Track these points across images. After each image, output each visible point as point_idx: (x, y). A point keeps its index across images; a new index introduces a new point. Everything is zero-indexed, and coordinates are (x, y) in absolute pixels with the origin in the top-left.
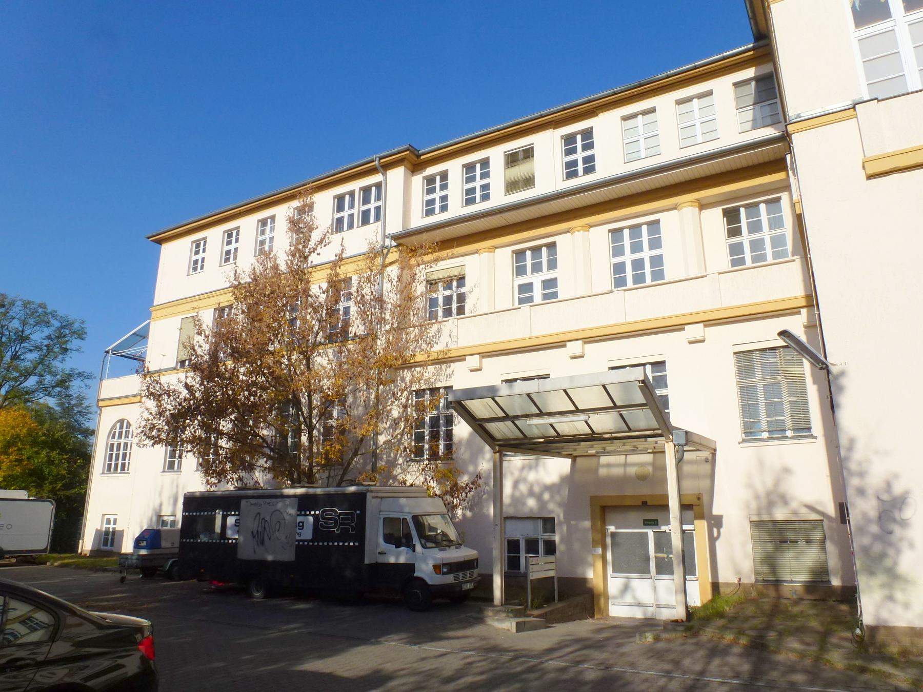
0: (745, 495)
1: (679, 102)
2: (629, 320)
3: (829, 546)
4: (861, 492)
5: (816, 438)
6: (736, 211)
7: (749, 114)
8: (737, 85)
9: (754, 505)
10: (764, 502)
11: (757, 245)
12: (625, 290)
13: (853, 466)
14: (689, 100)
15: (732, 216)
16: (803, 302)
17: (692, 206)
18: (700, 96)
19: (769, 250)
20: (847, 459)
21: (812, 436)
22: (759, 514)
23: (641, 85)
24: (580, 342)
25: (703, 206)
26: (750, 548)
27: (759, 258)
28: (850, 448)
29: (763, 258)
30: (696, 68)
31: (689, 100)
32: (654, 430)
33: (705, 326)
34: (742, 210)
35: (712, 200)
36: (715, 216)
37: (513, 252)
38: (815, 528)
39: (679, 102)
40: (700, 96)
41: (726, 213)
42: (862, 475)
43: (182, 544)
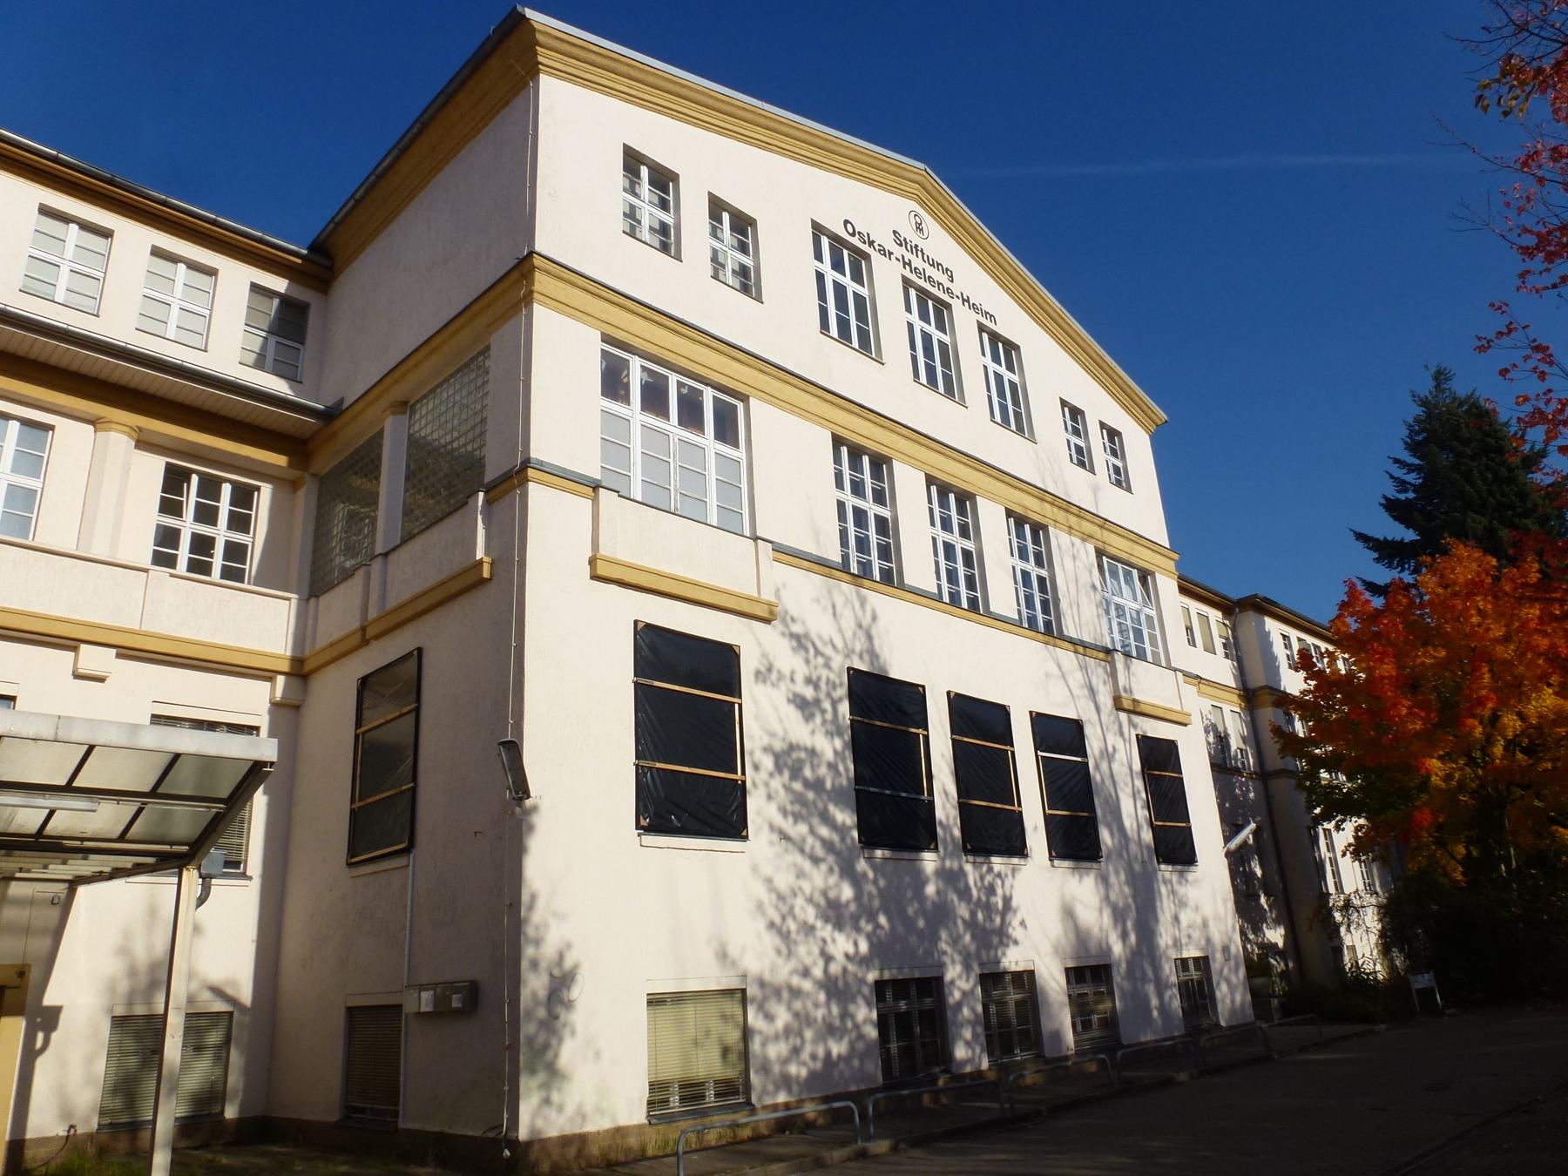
0: (112, 966)
1: (157, 252)
2: (146, 628)
3: (235, 1057)
4: (535, 965)
5: (250, 878)
6: (185, 475)
7: (256, 344)
8: (256, 288)
9: (123, 986)
10: (143, 980)
11: (202, 545)
12: (172, 575)
13: (530, 931)
14: (173, 259)
15: (174, 480)
16: (286, 668)
17: (129, 435)
18: (193, 266)
19: (218, 561)
20: (527, 921)
21: (244, 876)
22: (130, 1004)
23: (111, 182)
24: (114, 651)
25: (145, 443)
26: (100, 1066)
27: (199, 567)
28: (531, 907)
29: (205, 569)
30: (164, 204)
31: (173, 259)
32: (171, 844)
33: (119, 656)
34: (195, 479)
35: (161, 442)
36: (154, 467)
37: (168, 464)
38: (215, 1025)
39: (157, 252)
40: (193, 266)
41: (170, 468)
42: (537, 942)
43: (1006, 972)
